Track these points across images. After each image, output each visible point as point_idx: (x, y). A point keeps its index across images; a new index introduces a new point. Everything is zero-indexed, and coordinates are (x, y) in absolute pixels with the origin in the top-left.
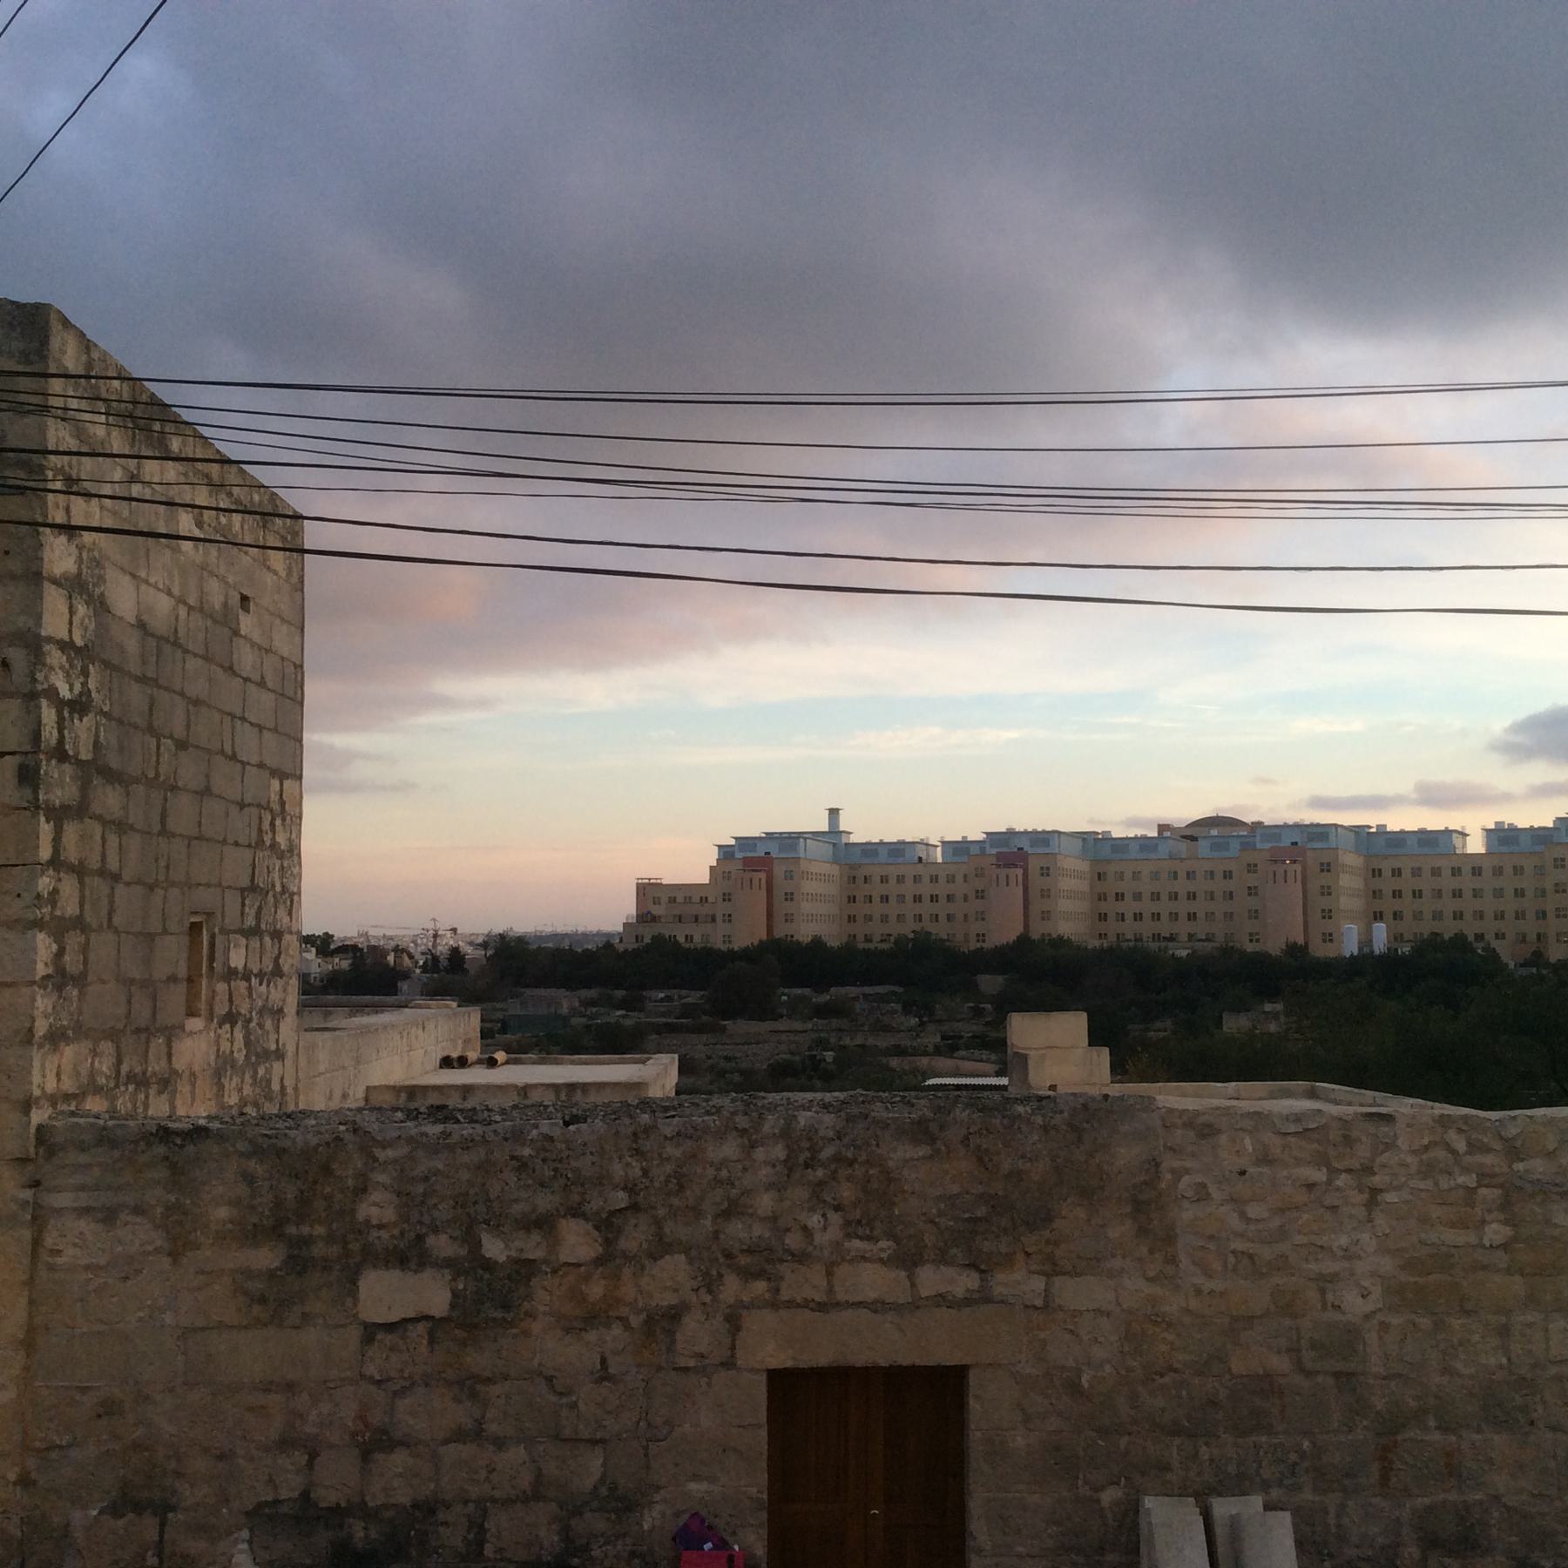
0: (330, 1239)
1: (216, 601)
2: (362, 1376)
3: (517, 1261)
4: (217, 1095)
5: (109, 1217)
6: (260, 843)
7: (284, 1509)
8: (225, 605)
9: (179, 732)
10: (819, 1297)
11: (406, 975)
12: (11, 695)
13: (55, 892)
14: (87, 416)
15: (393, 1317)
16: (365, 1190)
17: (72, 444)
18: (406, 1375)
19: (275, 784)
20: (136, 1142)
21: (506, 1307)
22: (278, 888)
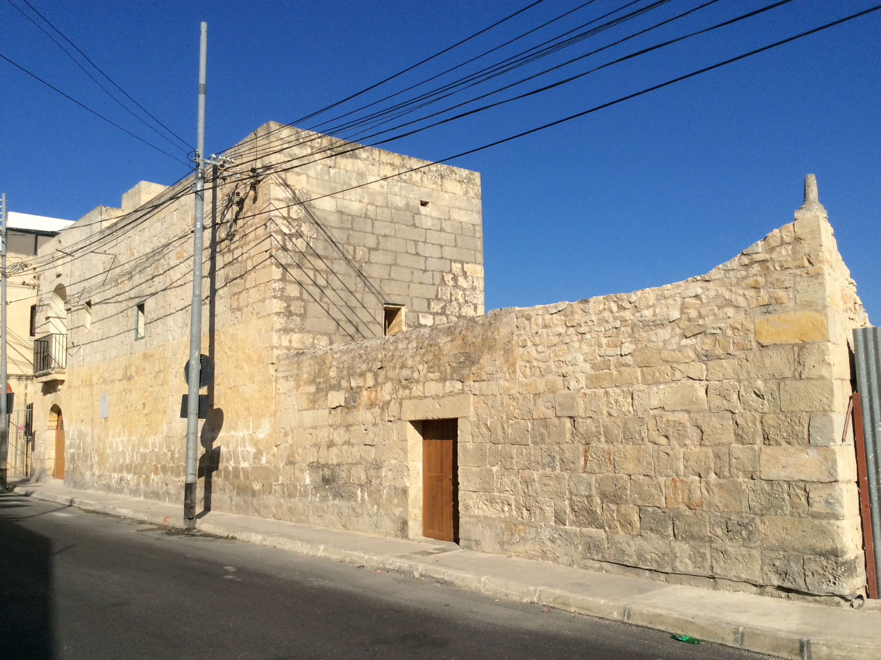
10: (420, 394)
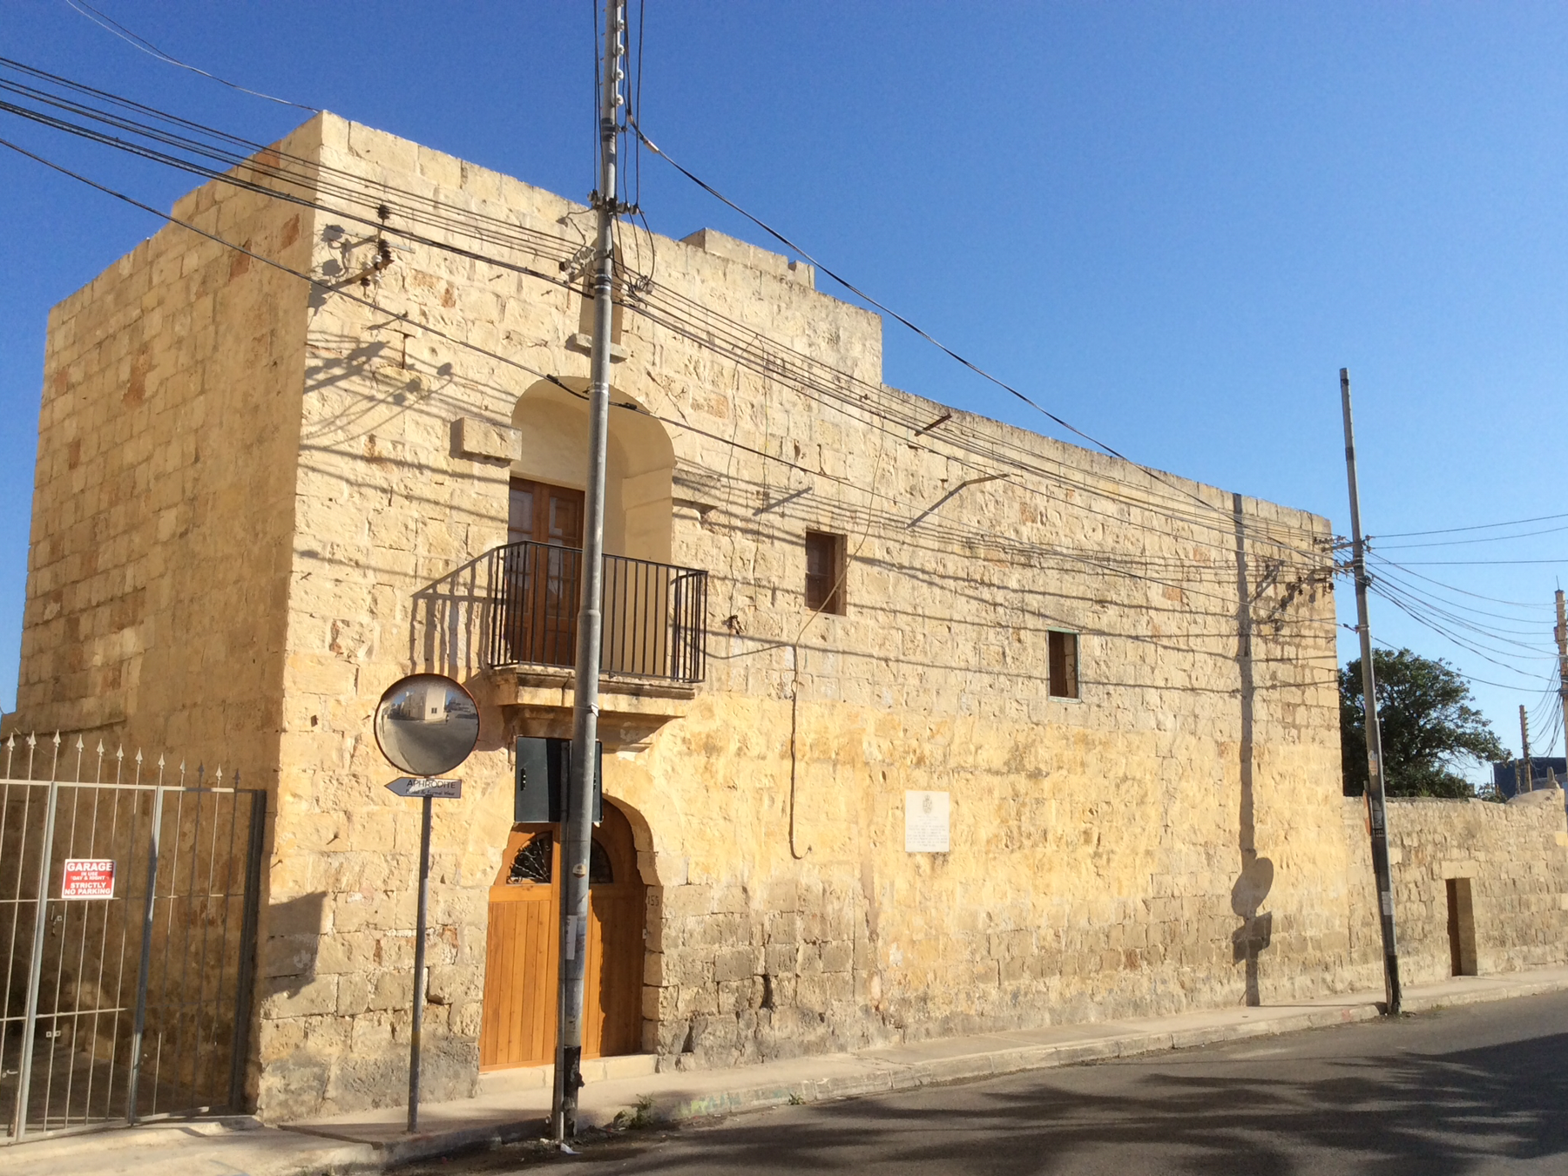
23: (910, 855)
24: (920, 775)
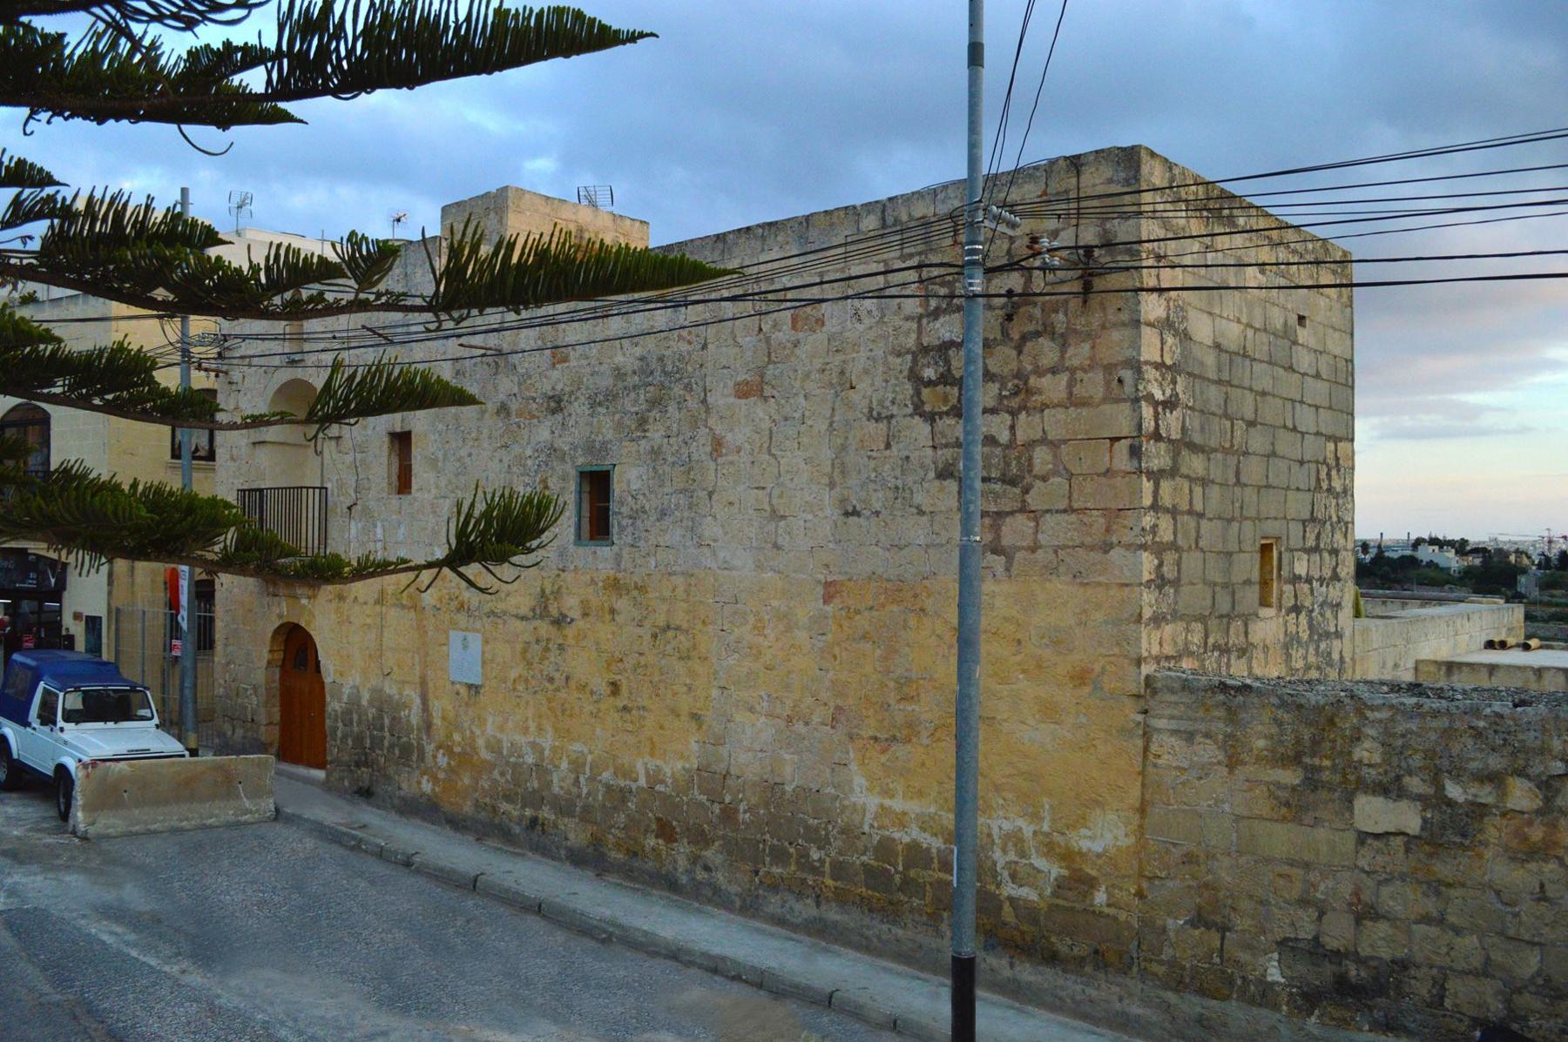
0: (1334, 768)
1: (1279, 324)
2: (1356, 866)
3: (1473, 803)
4: (1286, 661)
5: (1190, 737)
6: (1318, 487)
7: (1301, 945)
8: (1286, 323)
9: (1249, 415)
11: (1524, 571)
12: (1124, 400)
13: (1155, 526)
14: (1171, 214)
15: (1380, 831)
16: (1358, 739)
17: (1161, 234)
18: (1388, 870)
19: (1331, 446)
20: (1206, 691)
21: (1464, 836)
22: (1335, 519)
23: (453, 683)
24: (462, 619)
